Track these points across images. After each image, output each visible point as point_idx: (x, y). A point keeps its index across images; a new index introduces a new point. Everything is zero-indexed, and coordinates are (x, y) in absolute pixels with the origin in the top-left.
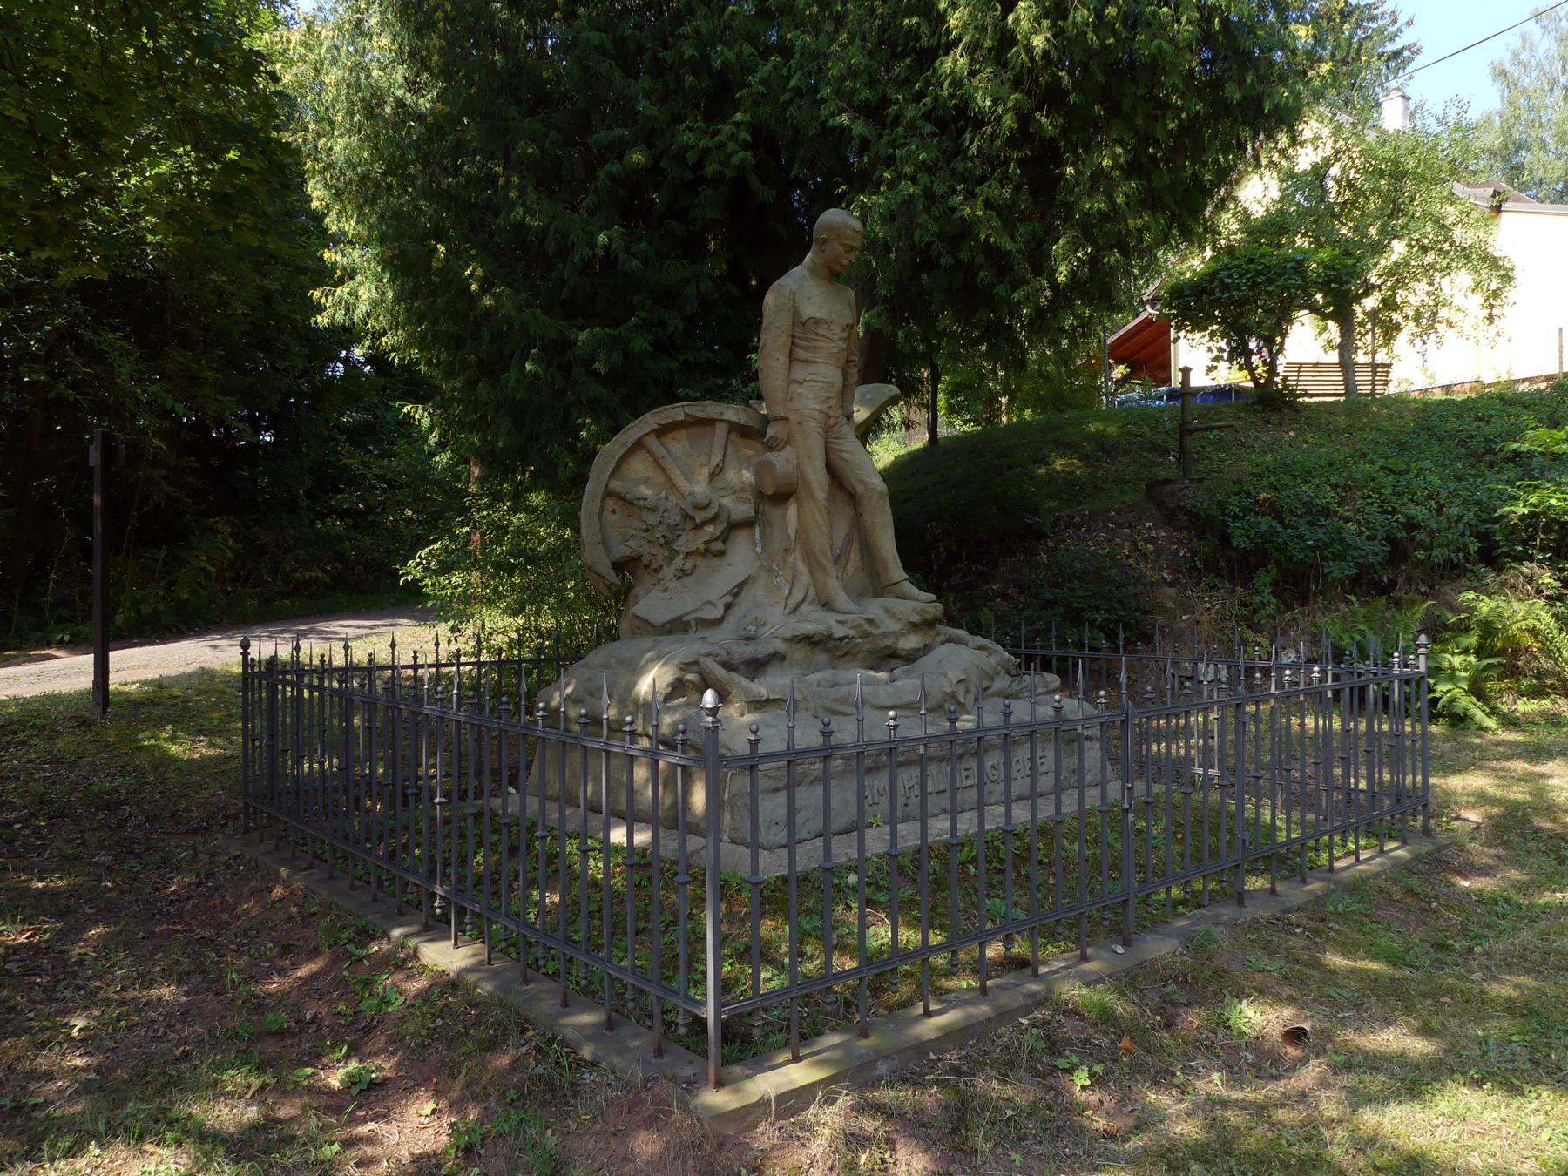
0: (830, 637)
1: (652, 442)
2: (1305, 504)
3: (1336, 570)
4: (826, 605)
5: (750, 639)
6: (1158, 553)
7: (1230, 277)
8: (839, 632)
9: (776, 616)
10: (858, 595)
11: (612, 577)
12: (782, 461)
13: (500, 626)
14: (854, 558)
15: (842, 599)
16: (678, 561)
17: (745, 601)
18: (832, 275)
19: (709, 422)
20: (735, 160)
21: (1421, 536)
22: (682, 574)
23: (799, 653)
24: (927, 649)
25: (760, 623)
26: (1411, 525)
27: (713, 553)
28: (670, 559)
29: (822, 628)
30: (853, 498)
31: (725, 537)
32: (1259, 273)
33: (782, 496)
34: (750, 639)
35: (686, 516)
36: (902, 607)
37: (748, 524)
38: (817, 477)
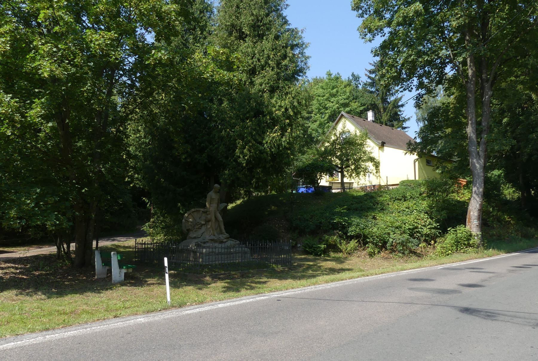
4: (214, 235)
9: (207, 237)
12: (209, 216)
13: (160, 238)
15: (216, 235)
18: (216, 192)
22: (195, 231)
26: (321, 223)
27: (200, 228)
30: (218, 221)
33: (209, 221)
36: (224, 236)
38: (213, 218)
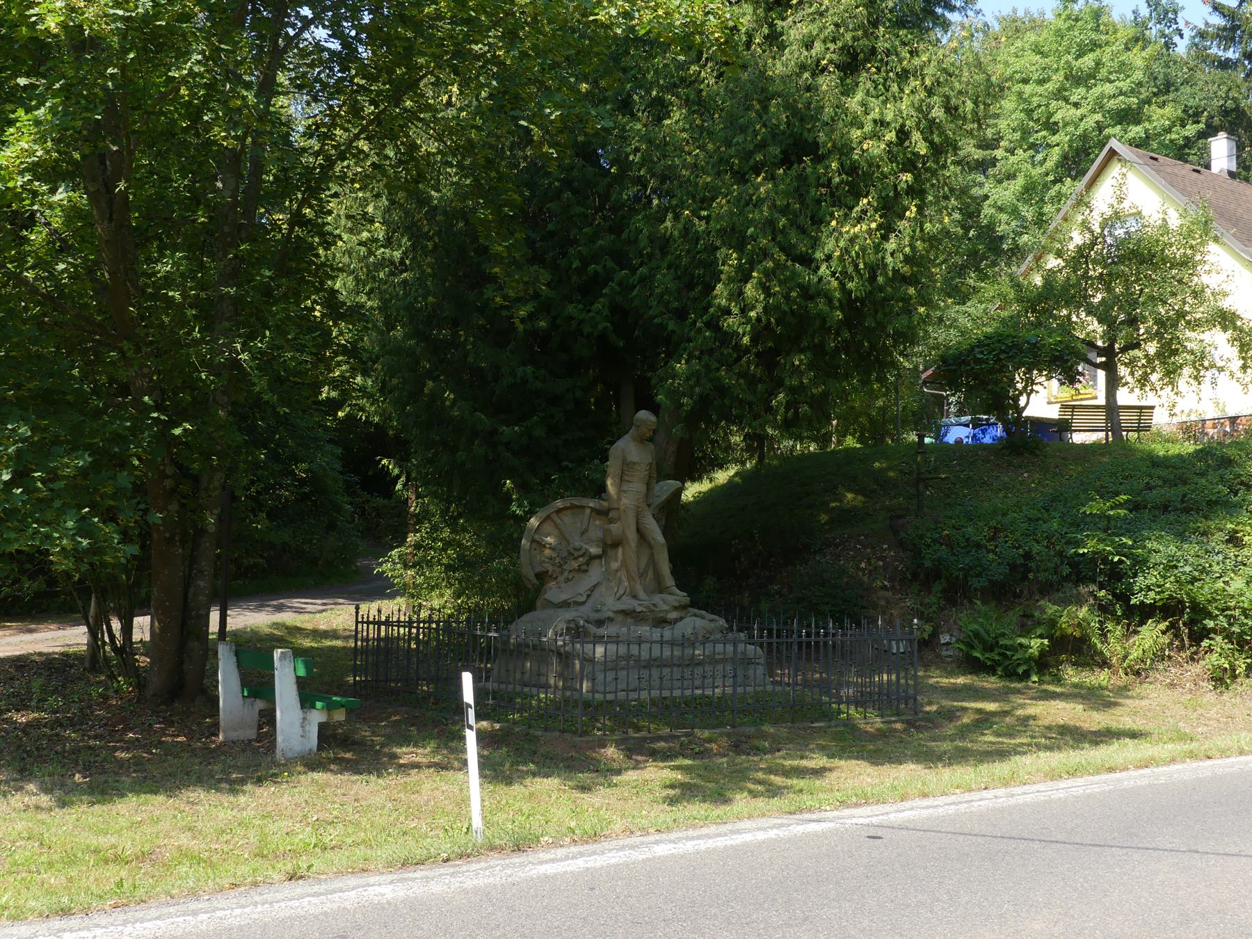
0: (634, 611)
1: (555, 517)
2: (968, 540)
3: (976, 583)
4: (635, 597)
5: (597, 611)
6: (885, 568)
7: (982, 353)
8: (639, 609)
9: (610, 602)
10: (650, 593)
11: (535, 581)
12: (615, 528)
14: (650, 574)
15: (642, 594)
16: (566, 574)
17: (596, 593)
18: (642, 440)
19: (583, 507)
20: (601, 327)
21: (1033, 565)
22: (567, 580)
23: (620, 618)
24: (682, 618)
25: (603, 604)
27: (582, 570)
28: (562, 573)
29: (630, 607)
30: (650, 546)
31: (588, 563)
32: (1003, 352)
33: (616, 545)
34: (597, 611)
35: (570, 553)
37: (599, 557)
38: (632, 536)
